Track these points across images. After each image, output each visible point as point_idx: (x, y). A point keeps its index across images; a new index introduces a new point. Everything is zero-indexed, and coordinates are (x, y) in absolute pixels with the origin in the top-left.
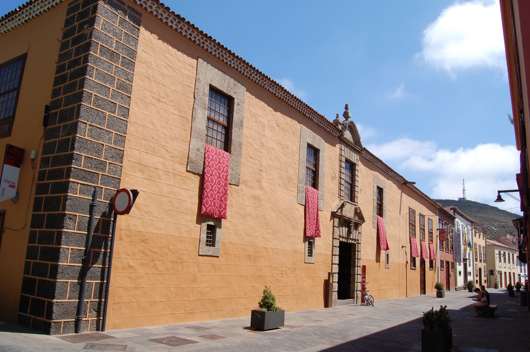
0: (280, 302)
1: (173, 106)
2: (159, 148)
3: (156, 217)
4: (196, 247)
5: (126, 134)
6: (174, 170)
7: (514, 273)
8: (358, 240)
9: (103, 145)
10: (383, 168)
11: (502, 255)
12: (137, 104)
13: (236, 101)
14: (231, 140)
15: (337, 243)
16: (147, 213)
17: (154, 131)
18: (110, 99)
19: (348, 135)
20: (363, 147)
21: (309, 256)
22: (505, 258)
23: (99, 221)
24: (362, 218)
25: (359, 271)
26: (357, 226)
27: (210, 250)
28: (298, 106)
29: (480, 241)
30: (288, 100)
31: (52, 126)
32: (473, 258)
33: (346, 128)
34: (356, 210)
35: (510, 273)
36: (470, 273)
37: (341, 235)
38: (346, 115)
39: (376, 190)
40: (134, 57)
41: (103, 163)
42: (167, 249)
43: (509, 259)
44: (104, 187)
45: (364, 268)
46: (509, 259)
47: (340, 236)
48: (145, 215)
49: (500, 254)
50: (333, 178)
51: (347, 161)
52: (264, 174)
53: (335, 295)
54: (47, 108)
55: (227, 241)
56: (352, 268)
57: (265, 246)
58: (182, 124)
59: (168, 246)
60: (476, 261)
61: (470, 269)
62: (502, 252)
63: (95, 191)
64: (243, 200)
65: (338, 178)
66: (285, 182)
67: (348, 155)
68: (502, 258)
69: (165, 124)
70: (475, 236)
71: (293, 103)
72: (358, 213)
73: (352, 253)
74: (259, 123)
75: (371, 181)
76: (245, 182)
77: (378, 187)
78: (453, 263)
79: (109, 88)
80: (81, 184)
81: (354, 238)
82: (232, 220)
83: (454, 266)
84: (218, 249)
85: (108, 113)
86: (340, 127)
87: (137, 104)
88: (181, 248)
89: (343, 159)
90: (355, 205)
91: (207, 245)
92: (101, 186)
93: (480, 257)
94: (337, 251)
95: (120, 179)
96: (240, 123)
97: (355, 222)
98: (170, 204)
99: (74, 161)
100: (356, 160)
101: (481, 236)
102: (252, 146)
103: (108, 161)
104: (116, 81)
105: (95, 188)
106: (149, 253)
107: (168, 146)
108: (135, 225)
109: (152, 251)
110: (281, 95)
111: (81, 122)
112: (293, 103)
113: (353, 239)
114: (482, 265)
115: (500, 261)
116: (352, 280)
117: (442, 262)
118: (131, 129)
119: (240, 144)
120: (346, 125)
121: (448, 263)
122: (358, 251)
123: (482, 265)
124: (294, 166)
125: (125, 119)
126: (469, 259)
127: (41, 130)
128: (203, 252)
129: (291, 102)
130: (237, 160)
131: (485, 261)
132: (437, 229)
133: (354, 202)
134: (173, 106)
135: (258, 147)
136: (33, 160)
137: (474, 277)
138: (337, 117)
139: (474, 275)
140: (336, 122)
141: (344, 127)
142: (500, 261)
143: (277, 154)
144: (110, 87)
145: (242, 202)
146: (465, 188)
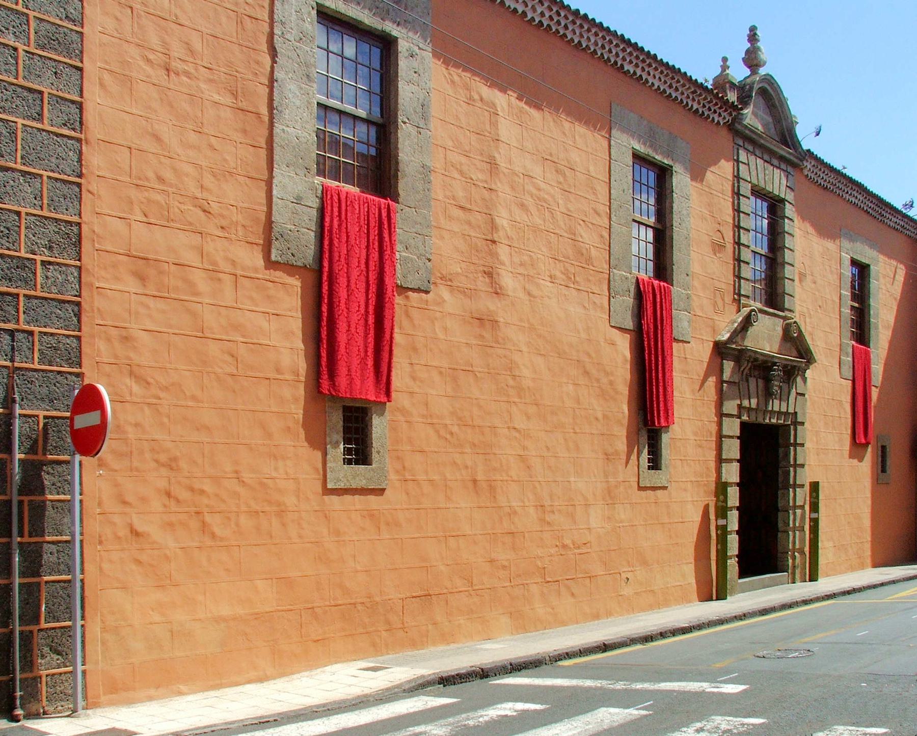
1: (211, 81)
2: (183, 207)
3: (194, 398)
4: (317, 470)
5: (80, 176)
6: (234, 263)
9: (18, 214)
10: (868, 205)
12: (102, 85)
14: (397, 163)
15: (732, 427)
16: (165, 389)
17: (163, 159)
18: (21, 81)
19: (753, 117)
20: (805, 147)
21: (649, 468)
23: (45, 449)
24: (805, 355)
25: (801, 496)
26: (791, 373)
27: (358, 475)
28: (596, 44)
30: (566, 27)
33: (750, 97)
34: (787, 330)
38: (752, 60)
39: (848, 271)
41: (23, 264)
42: (236, 481)
44: (37, 329)
45: (815, 487)
48: (162, 395)
50: (718, 247)
51: (758, 192)
53: (733, 565)
56: (780, 492)
57: (522, 453)
58: (245, 132)
59: (236, 472)
64: (445, 329)
65: (730, 247)
66: (572, 270)
67: (761, 176)
69: (193, 137)
71: (581, 36)
72: (794, 340)
73: (781, 450)
74: (479, 104)
76: (447, 280)
79: (15, 49)
82: (417, 390)
85: (20, 121)
86: (732, 97)
87: (102, 85)
88: (274, 474)
89: (746, 189)
90: (785, 318)
91: (349, 462)
92: (27, 327)
94: (733, 449)
96: (419, 109)
97: (785, 366)
98: (228, 358)
100: (783, 188)
103: (38, 258)
104: (33, 24)
106: (184, 495)
107: (210, 198)
108: (137, 425)
109: (192, 490)
110: (542, 15)
112: (581, 36)
116: (780, 524)
118: (95, 159)
120: (751, 88)
124: (597, 220)
125: (73, 134)
128: (339, 480)
129: (574, 32)
130: (419, 219)
133: (783, 310)
134: (211, 81)
135: (480, 176)
138: (725, 67)
140: (722, 82)
141: (745, 99)
143: (539, 190)
144: (17, 44)
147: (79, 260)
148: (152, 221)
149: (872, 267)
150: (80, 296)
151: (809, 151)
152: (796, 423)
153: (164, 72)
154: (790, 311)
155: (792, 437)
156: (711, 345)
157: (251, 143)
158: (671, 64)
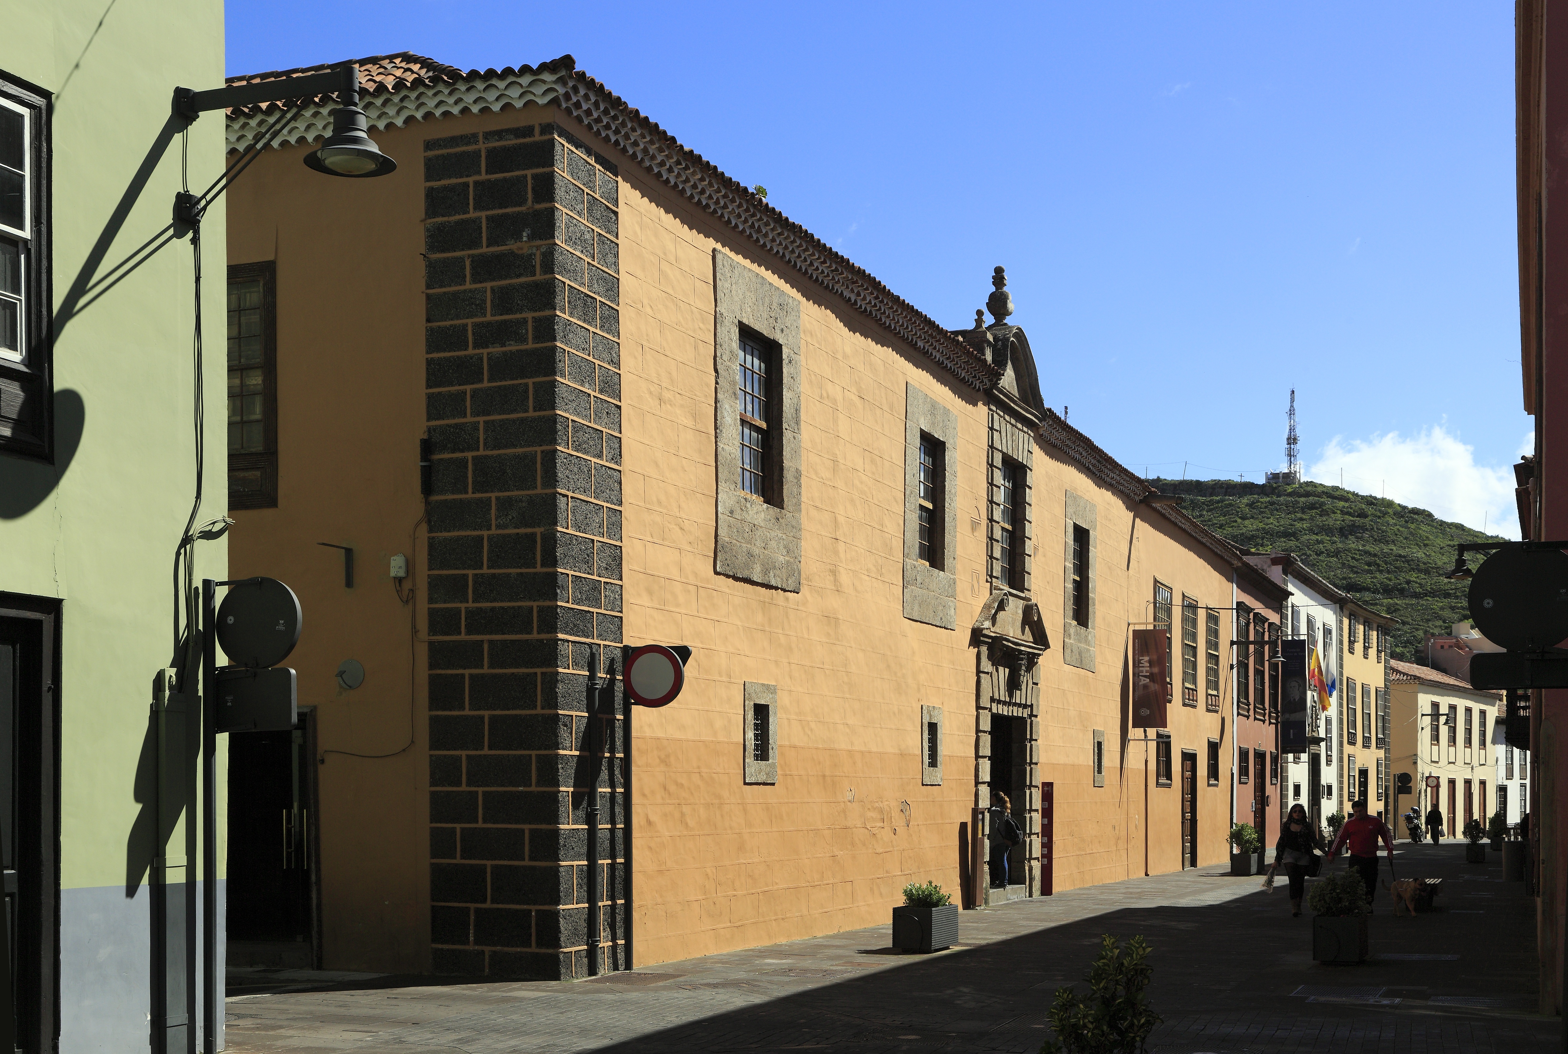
0: (881, 894)
7: (1483, 783)
8: (1031, 706)
11: (1443, 719)
13: (785, 351)
15: (986, 725)
22: (1453, 731)
24: (1041, 639)
29: (1367, 669)
31: (450, 497)
32: (1341, 736)
35: (1468, 783)
36: (1330, 788)
37: (996, 696)
38: (998, 304)
40: (616, 298)
42: (698, 775)
43: (1469, 731)
45: (1048, 790)
46: (1469, 731)
47: (992, 700)
49: (1435, 714)
50: (975, 525)
52: (841, 547)
54: (427, 447)
55: (787, 743)
57: (850, 748)
60: (1352, 742)
61: (1329, 775)
62: (1444, 709)
63: (593, 655)
65: (984, 522)
68: (1444, 731)
70: (1351, 651)
72: (1032, 620)
75: (1059, 511)
77: (1077, 528)
78: (1275, 759)
80: (572, 642)
81: (1023, 702)
83: (1279, 773)
84: (773, 766)
89: (998, 460)
93: (1367, 727)
95: (621, 618)
99: (558, 591)
101: (1373, 652)
102: (816, 473)
105: (591, 648)
111: (560, 494)
113: (1019, 705)
114: (1368, 758)
115: (1435, 738)
117: (1243, 755)
119: (798, 474)
121: (1260, 756)
122: (1031, 740)
123: (1368, 758)
126: (1328, 740)
127: (415, 506)
131: (1380, 743)
132: (1232, 643)
136: (399, 580)
137: (1341, 803)
139: (1341, 796)
142: (1435, 738)
145: (806, 636)
146: (1298, 432)
147: (621, 580)
148: (655, 540)
149: (1091, 532)
150: (621, 612)
151: (1050, 410)
152: (1031, 715)
153: (658, 401)
154: (1029, 590)
155: (1028, 733)
156: (970, 631)
157: (704, 462)
158: (652, 120)
